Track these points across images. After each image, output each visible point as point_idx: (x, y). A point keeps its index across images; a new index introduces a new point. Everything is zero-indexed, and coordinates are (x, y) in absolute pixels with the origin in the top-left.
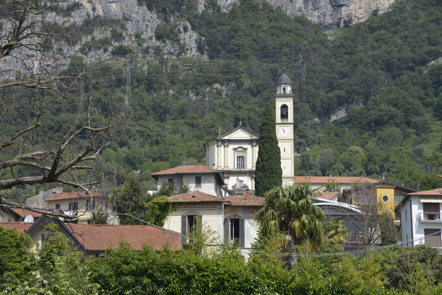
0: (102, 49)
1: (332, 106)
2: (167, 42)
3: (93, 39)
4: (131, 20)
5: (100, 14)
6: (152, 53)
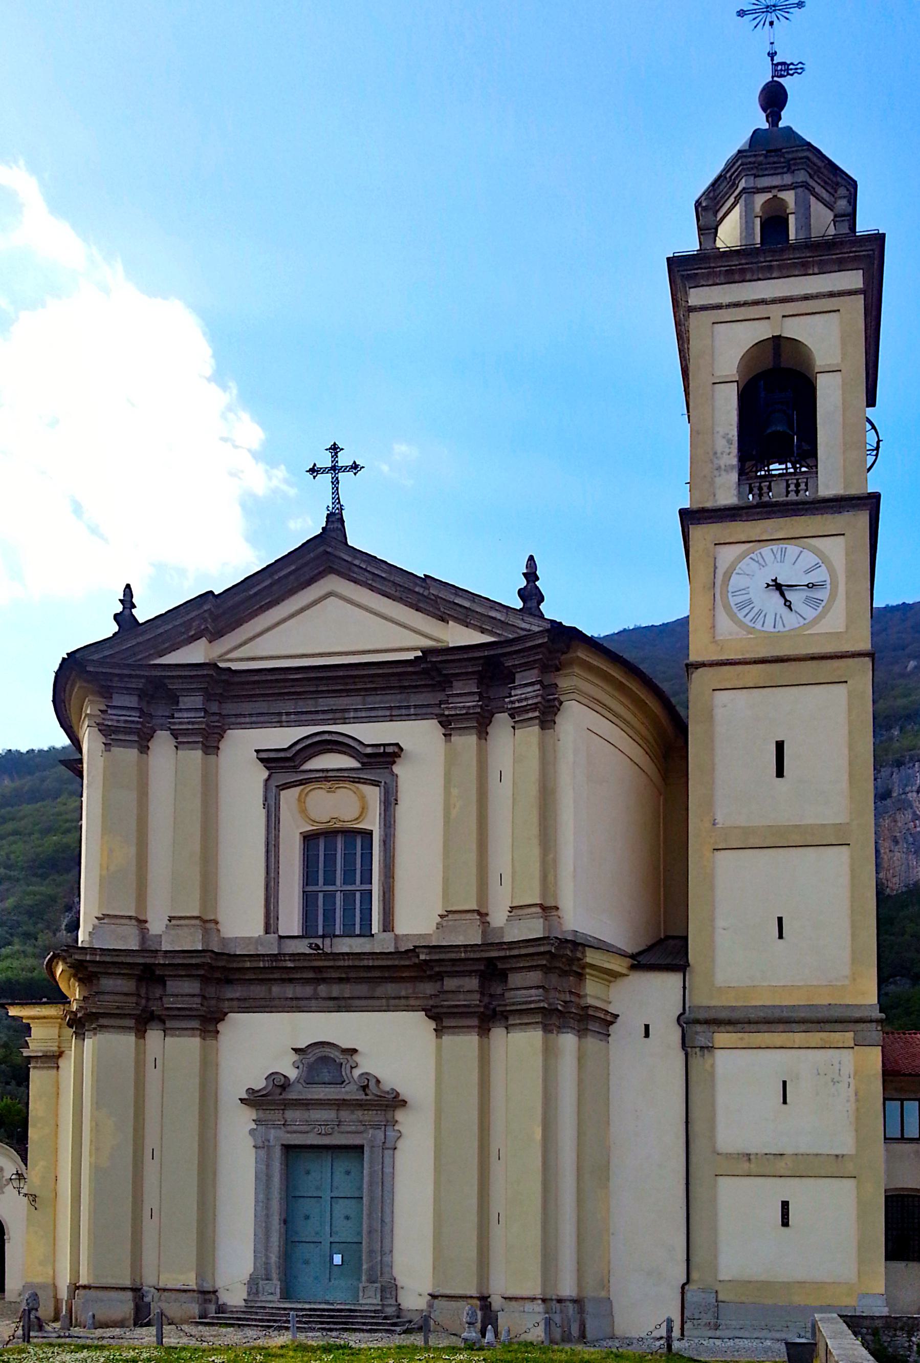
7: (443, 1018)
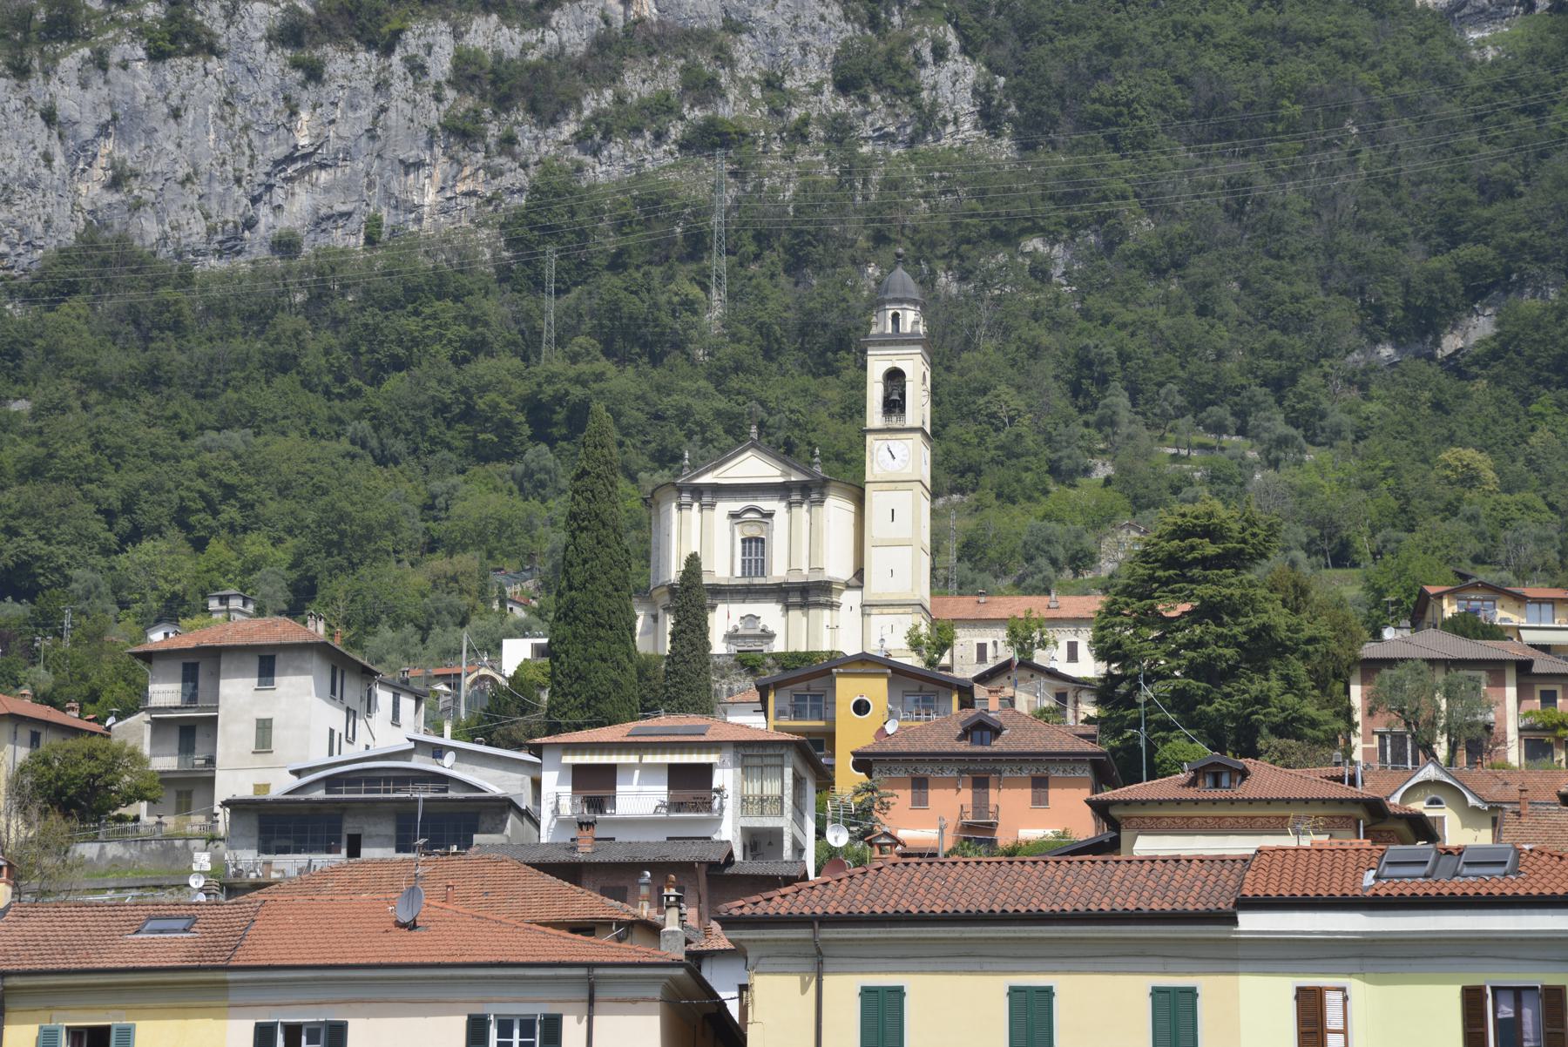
0: (647, 134)
1: (1442, 300)
2: (875, 98)
3: (620, 100)
4: (750, 31)
5: (646, 13)
6: (818, 139)
7: (788, 607)
